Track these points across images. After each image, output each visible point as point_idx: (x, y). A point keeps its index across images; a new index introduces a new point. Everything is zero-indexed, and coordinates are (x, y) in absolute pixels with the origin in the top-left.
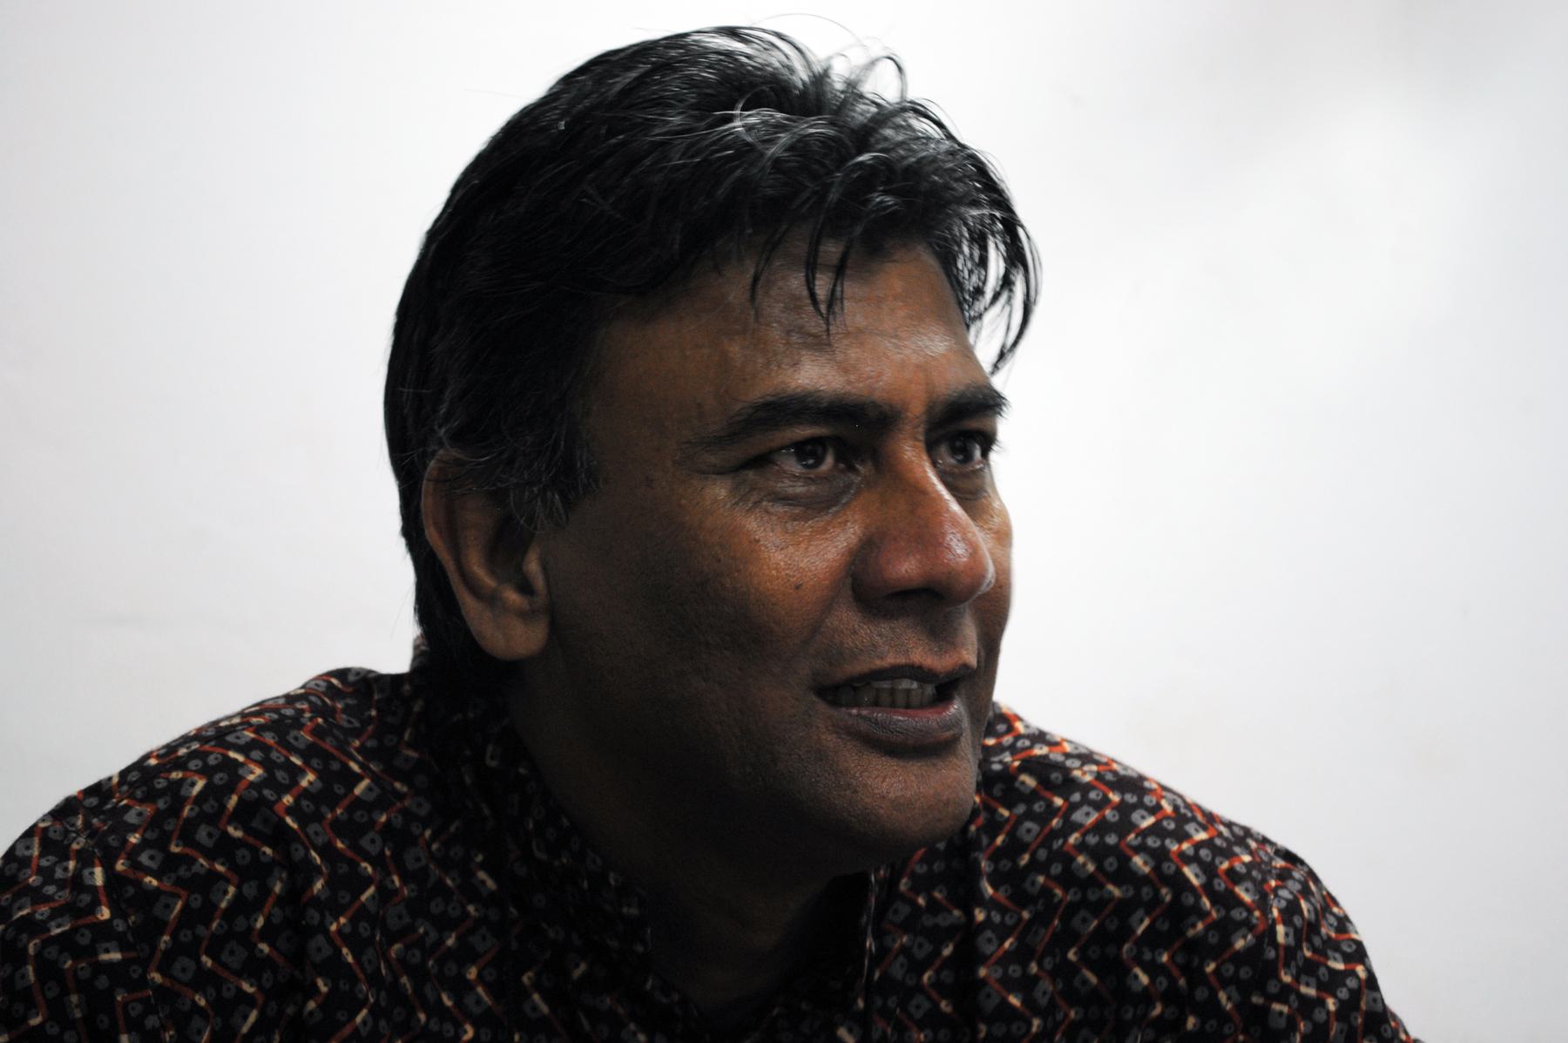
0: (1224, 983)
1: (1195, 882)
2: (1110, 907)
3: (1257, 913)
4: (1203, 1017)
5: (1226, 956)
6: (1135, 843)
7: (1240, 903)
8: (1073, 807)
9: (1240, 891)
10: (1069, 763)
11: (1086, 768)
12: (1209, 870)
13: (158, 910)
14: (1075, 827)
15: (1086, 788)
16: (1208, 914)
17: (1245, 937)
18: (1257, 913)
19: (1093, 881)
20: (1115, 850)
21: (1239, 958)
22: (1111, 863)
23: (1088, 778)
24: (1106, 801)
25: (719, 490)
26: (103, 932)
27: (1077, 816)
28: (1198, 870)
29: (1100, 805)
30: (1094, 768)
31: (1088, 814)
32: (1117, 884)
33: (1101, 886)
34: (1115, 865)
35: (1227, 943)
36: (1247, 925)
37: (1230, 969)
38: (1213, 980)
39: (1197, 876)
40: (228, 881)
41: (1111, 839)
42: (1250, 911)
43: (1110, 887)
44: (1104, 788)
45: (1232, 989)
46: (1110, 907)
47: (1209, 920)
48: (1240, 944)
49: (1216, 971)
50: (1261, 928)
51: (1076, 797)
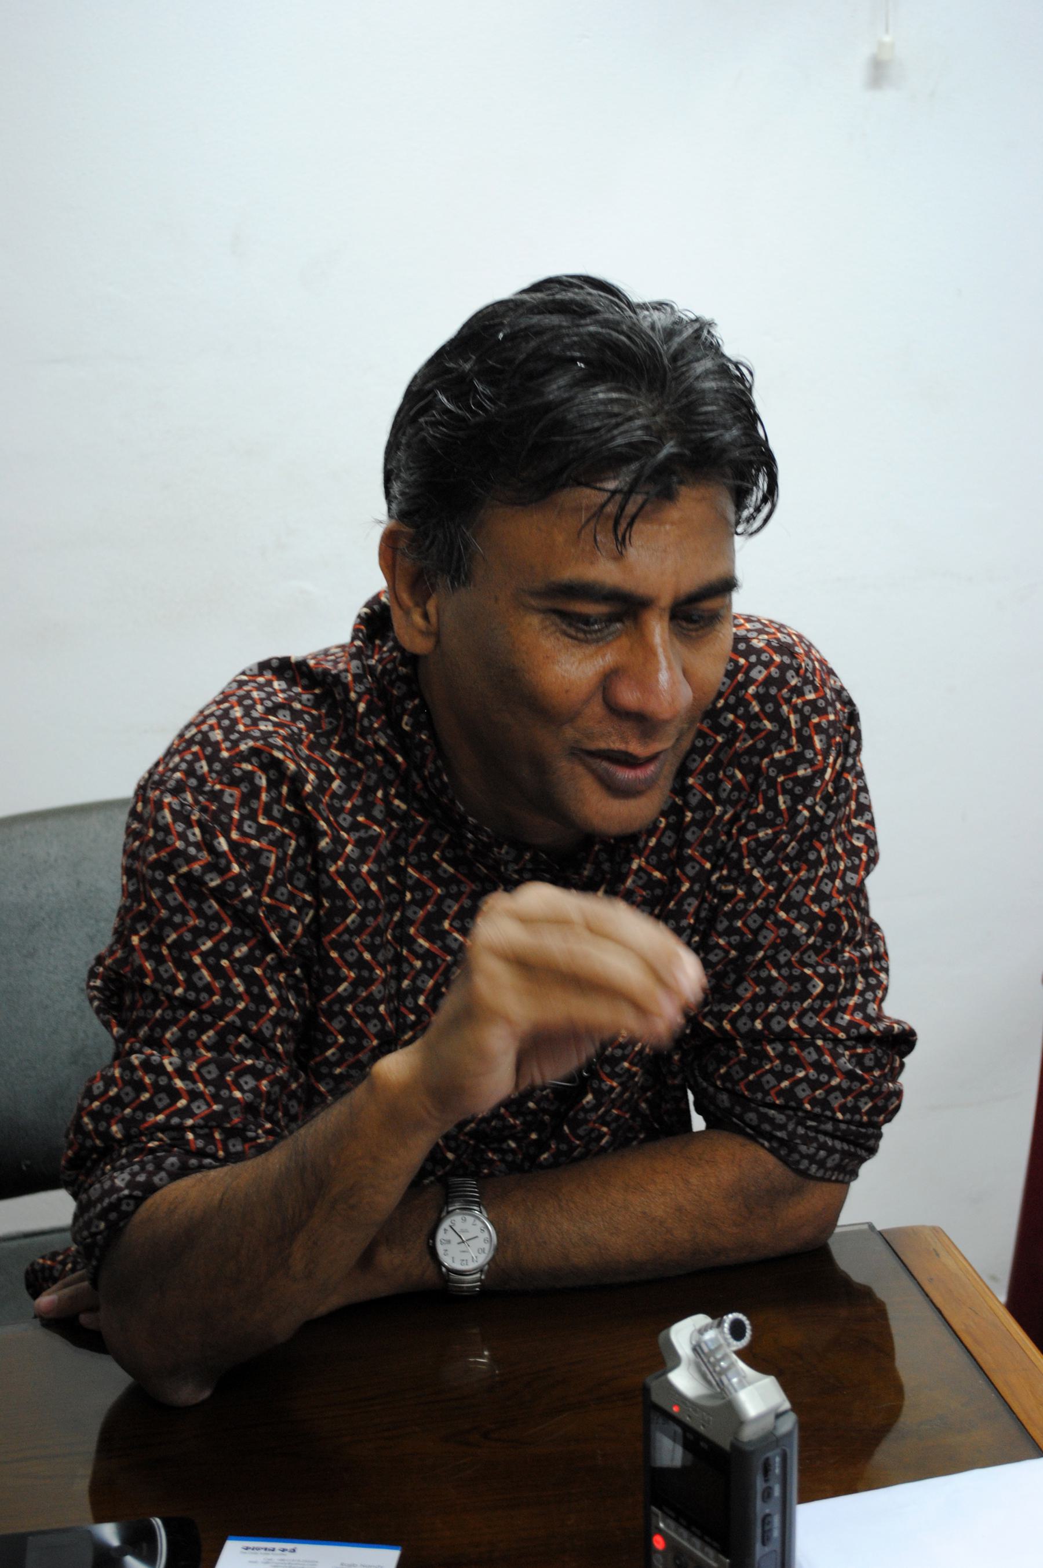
0: (785, 792)
1: (793, 726)
2: (763, 734)
3: (820, 758)
4: (767, 808)
5: (791, 776)
6: (786, 696)
7: (812, 746)
8: (751, 666)
9: (816, 739)
10: (750, 635)
11: (760, 637)
12: (805, 720)
13: (263, 861)
14: (753, 681)
15: (759, 652)
16: (792, 747)
17: (805, 769)
18: (820, 758)
19: (756, 717)
20: (774, 699)
21: (797, 781)
22: (770, 707)
23: (761, 645)
24: (772, 660)
25: (535, 621)
26: (238, 880)
27: (754, 674)
28: (798, 720)
29: (767, 665)
30: (766, 637)
31: (760, 672)
32: (770, 721)
33: (761, 721)
34: (772, 710)
35: (794, 768)
36: (811, 763)
37: (790, 785)
38: (779, 787)
39: (796, 722)
40: (291, 838)
41: (773, 691)
42: (816, 754)
43: (766, 722)
44: (771, 651)
45: (788, 797)
46: (763, 734)
47: (791, 751)
48: (801, 772)
49: (782, 783)
50: (818, 767)
51: (753, 659)
